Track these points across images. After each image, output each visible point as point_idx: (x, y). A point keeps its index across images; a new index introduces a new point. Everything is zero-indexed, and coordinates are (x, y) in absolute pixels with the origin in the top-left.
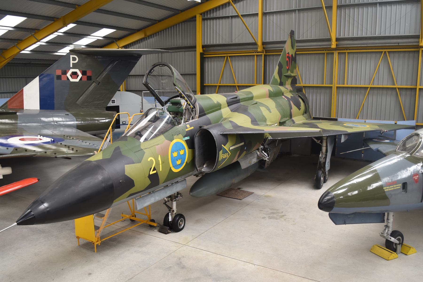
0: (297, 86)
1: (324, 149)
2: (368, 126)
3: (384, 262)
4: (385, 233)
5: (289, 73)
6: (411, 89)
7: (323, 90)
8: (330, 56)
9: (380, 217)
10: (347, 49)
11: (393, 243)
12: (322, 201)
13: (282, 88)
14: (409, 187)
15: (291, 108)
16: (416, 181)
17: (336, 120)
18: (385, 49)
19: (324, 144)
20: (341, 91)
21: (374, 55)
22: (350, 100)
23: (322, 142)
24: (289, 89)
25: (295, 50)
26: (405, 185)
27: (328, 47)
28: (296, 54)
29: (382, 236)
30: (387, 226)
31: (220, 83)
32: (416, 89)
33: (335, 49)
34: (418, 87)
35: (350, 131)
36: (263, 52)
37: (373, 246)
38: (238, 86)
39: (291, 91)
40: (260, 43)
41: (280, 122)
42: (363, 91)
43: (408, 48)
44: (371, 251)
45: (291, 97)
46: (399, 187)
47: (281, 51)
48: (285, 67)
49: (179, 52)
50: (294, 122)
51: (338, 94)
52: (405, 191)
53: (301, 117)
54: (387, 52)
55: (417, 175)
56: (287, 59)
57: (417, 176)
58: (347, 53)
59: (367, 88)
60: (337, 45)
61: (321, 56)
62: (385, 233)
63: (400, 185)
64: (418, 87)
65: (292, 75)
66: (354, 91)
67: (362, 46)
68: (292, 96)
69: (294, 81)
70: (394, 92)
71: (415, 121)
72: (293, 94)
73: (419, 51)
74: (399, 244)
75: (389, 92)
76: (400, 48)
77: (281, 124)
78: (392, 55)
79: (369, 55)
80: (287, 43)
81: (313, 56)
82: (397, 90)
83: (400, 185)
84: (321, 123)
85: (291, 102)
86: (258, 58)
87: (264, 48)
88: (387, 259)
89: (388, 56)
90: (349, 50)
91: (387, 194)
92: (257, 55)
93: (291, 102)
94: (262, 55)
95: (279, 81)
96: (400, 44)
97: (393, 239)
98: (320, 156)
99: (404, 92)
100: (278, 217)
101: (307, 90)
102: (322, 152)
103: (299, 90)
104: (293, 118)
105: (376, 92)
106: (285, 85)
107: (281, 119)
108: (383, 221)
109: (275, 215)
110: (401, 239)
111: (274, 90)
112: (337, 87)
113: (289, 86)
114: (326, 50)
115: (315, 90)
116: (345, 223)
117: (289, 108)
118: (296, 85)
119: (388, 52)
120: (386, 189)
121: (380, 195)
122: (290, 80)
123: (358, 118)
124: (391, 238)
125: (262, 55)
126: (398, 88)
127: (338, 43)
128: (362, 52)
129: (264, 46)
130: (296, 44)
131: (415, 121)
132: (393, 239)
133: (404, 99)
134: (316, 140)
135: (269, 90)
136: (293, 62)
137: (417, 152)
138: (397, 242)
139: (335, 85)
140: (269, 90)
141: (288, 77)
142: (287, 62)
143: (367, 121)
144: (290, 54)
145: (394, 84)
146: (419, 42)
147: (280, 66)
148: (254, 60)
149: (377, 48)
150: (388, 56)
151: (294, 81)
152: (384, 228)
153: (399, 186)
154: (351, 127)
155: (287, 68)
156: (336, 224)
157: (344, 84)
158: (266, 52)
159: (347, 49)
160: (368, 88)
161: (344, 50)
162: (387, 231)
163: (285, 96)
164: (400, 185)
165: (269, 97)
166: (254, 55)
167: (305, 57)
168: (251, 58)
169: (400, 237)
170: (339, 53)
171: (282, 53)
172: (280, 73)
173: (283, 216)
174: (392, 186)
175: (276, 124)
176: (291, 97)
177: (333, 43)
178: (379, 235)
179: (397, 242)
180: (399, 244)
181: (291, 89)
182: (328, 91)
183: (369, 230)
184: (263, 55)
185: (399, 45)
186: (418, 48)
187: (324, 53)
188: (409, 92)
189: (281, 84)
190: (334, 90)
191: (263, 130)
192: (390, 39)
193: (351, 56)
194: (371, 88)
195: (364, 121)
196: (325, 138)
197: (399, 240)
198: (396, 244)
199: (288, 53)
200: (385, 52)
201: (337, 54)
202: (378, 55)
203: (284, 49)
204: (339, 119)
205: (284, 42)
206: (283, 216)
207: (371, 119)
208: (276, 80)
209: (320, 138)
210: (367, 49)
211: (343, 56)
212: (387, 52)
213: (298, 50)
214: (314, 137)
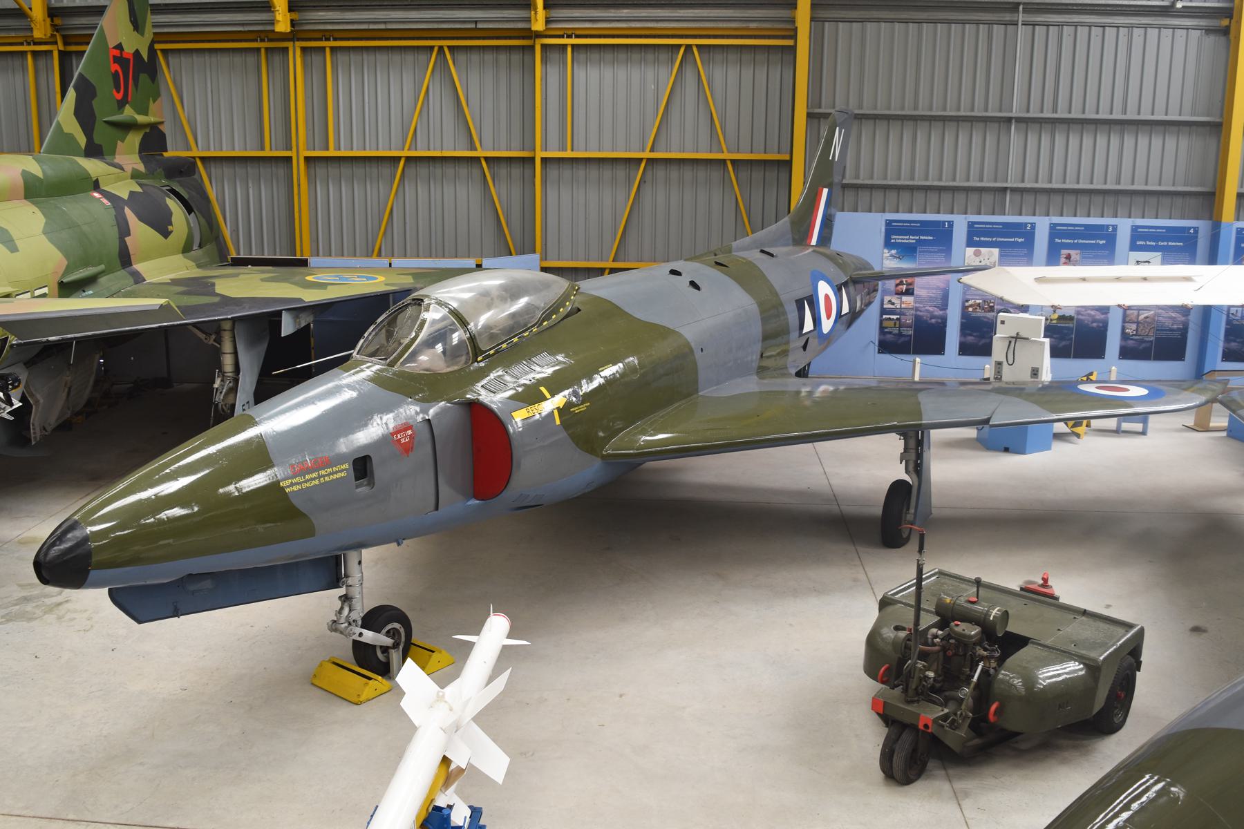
0: (170, 159)
1: (228, 361)
2: (381, 279)
3: (344, 711)
4: (342, 620)
5: (129, 113)
6: (523, 160)
7: (265, 170)
8: (277, 59)
9: (330, 571)
10: (327, 35)
11: (374, 647)
12: (46, 554)
13: (93, 167)
14: (379, 472)
15: (124, 231)
16: (407, 449)
17: (304, 263)
18: (439, 38)
19: (227, 347)
20: (320, 171)
21: (409, 57)
22: (349, 198)
23: (219, 340)
24: (129, 169)
25: (149, 32)
26: (362, 466)
27: (520, 25)
28: (152, 50)
29: (336, 630)
30: (346, 599)
31: (652, 150)
32: (532, 159)
33: (293, 36)
34: (540, 154)
35: (311, 297)
36: (56, 43)
37: (321, 665)
38: (733, 162)
39: (135, 175)
40: (38, 12)
41: (62, 285)
42: (386, 170)
43: (769, 37)
44: (313, 681)
45: (132, 193)
46: (343, 474)
47: (86, 39)
48: (106, 94)
49: (942, 22)
50: (138, 278)
51: (312, 180)
52: (369, 484)
53: (179, 259)
54: (446, 49)
55: (406, 429)
56: (117, 67)
57: (410, 432)
58: (569, 49)
59: (396, 159)
60: (293, 23)
61: (251, 59)
62: (342, 620)
63: (343, 467)
64: (540, 154)
65: (141, 119)
66: (359, 170)
67: (372, 27)
68: (139, 189)
69: (153, 141)
70: (476, 172)
71: (537, 256)
72: (140, 185)
73: (532, 48)
74: (395, 646)
75: (463, 170)
76: (484, 38)
77: (67, 289)
78: (462, 57)
79: (396, 58)
80: (108, 14)
81: (225, 60)
82: (484, 163)
83: (345, 466)
84: (237, 275)
85: (128, 211)
86: (42, 63)
87: (56, 28)
88: (355, 699)
89: (450, 62)
90: (335, 39)
91: (296, 502)
92: (34, 53)
93: (128, 211)
94: (51, 52)
95: (82, 140)
96: (479, 26)
97: (369, 636)
98: (216, 386)
99: (503, 171)
100: (38, 612)
101: (213, 170)
102: (222, 374)
103: (183, 170)
104: (139, 267)
105: (423, 170)
106: (113, 153)
107: (68, 270)
108: (335, 582)
109: (29, 607)
110: (402, 631)
111: (50, 172)
112: (307, 159)
113: (129, 155)
114: (262, 40)
115: (240, 170)
116: (176, 613)
117: (113, 233)
118: (165, 154)
119: (697, 46)
120: (292, 485)
121: (275, 507)
122: (134, 139)
123: (379, 255)
124: (361, 634)
125: (51, 52)
126: (486, 159)
127: (295, 16)
128: (216, 50)
129: (58, 21)
130: (151, 19)
131: (537, 256)
132: (369, 636)
133: (503, 191)
134: (202, 336)
135: (25, 174)
136: (144, 78)
137: (406, 361)
138: (388, 641)
139: (302, 150)
140: (25, 174)
141: (127, 127)
142: (115, 76)
143: (398, 262)
144: (129, 49)
145: (473, 148)
146: (528, 20)
147: (86, 93)
148: (24, 69)
149: (491, 34)
150: (450, 62)
151: (153, 141)
152: (339, 604)
153: (343, 471)
154: (323, 286)
155: (120, 96)
156: (139, 622)
157: (327, 149)
158: (65, 44)
159: (327, 35)
160: (400, 158)
161: (320, 39)
162: (346, 610)
163: (106, 194)
164: (343, 467)
165: (26, 198)
166: (26, 52)
167: (197, 60)
168: (17, 62)
169: (397, 625)
170: (304, 49)
171: (89, 48)
172: (84, 114)
173: (60, 604)
174: (314, 475)
175: (45, 290)
176: (132, 193)
177: (279, 17)
178: (326, 627)
179: (388, 641)
180: (395, 646)
181: (141, 167)
182: (281, 171)
183: (296, 618)
184: (56, 54)
185: (476, 29)
186: (529, 38)
187: (259, 50)
188: (516, 171)
189: (93, 151)
190: (299, 168)
191: (300, 300)
192: (447, 9)
193: (342, 58)
194: (408, 159)
195: (386, 262)
196: (227, 326)
197: (392, 634)
198: (385, 650)
199: (119, 47)
200: (441, 48)
201: (298, 52)
202: (422, 57)
203: (96, 32)
204: (313, 261)
205: (99, 11)
206: (60, 604)
207: (405, 256)
208: (70, 137)
209: (215, 329)
210: (387, 39)
211: (316, 58)
212: (446, 49)
213: (158, 38)
214: (194, 325)
